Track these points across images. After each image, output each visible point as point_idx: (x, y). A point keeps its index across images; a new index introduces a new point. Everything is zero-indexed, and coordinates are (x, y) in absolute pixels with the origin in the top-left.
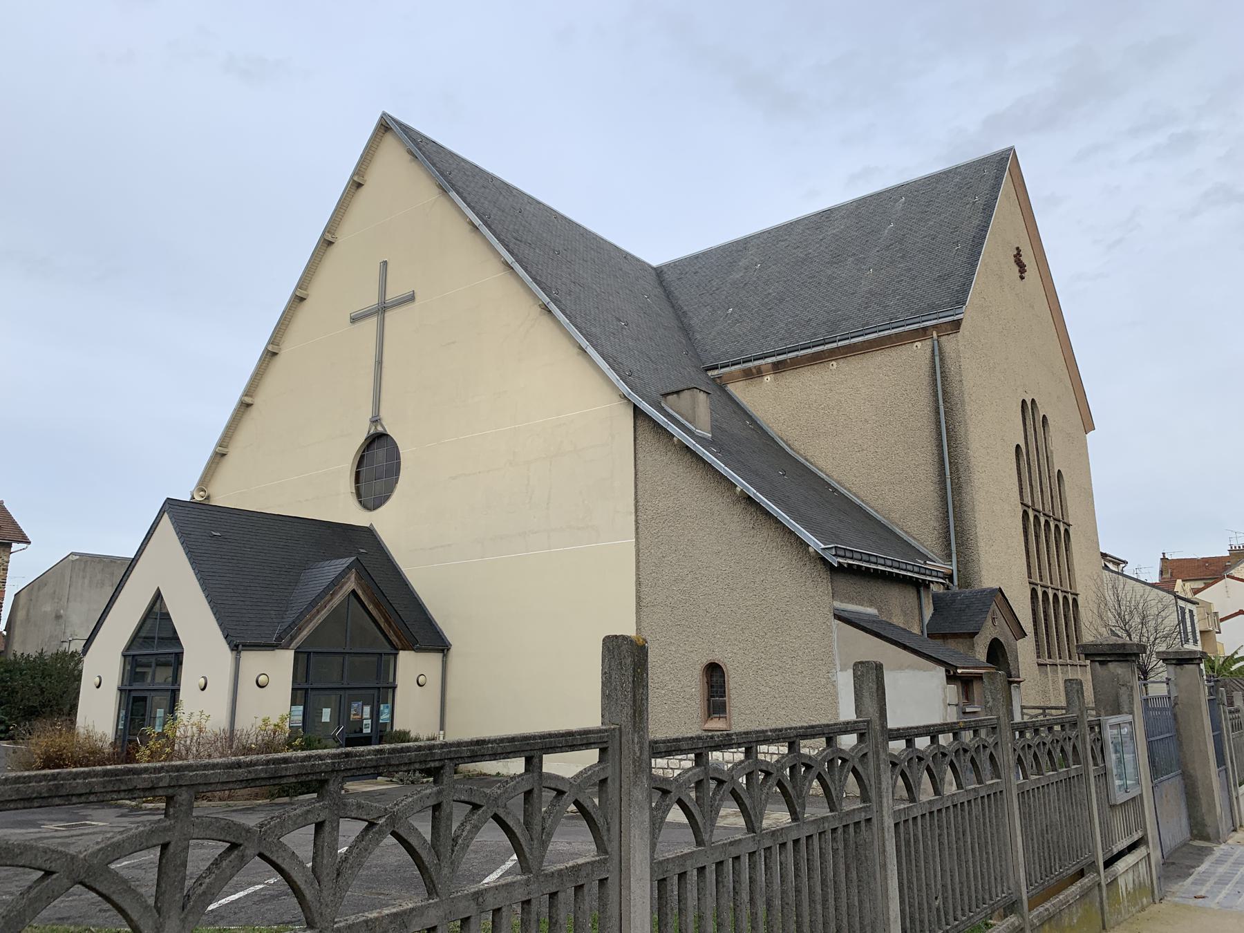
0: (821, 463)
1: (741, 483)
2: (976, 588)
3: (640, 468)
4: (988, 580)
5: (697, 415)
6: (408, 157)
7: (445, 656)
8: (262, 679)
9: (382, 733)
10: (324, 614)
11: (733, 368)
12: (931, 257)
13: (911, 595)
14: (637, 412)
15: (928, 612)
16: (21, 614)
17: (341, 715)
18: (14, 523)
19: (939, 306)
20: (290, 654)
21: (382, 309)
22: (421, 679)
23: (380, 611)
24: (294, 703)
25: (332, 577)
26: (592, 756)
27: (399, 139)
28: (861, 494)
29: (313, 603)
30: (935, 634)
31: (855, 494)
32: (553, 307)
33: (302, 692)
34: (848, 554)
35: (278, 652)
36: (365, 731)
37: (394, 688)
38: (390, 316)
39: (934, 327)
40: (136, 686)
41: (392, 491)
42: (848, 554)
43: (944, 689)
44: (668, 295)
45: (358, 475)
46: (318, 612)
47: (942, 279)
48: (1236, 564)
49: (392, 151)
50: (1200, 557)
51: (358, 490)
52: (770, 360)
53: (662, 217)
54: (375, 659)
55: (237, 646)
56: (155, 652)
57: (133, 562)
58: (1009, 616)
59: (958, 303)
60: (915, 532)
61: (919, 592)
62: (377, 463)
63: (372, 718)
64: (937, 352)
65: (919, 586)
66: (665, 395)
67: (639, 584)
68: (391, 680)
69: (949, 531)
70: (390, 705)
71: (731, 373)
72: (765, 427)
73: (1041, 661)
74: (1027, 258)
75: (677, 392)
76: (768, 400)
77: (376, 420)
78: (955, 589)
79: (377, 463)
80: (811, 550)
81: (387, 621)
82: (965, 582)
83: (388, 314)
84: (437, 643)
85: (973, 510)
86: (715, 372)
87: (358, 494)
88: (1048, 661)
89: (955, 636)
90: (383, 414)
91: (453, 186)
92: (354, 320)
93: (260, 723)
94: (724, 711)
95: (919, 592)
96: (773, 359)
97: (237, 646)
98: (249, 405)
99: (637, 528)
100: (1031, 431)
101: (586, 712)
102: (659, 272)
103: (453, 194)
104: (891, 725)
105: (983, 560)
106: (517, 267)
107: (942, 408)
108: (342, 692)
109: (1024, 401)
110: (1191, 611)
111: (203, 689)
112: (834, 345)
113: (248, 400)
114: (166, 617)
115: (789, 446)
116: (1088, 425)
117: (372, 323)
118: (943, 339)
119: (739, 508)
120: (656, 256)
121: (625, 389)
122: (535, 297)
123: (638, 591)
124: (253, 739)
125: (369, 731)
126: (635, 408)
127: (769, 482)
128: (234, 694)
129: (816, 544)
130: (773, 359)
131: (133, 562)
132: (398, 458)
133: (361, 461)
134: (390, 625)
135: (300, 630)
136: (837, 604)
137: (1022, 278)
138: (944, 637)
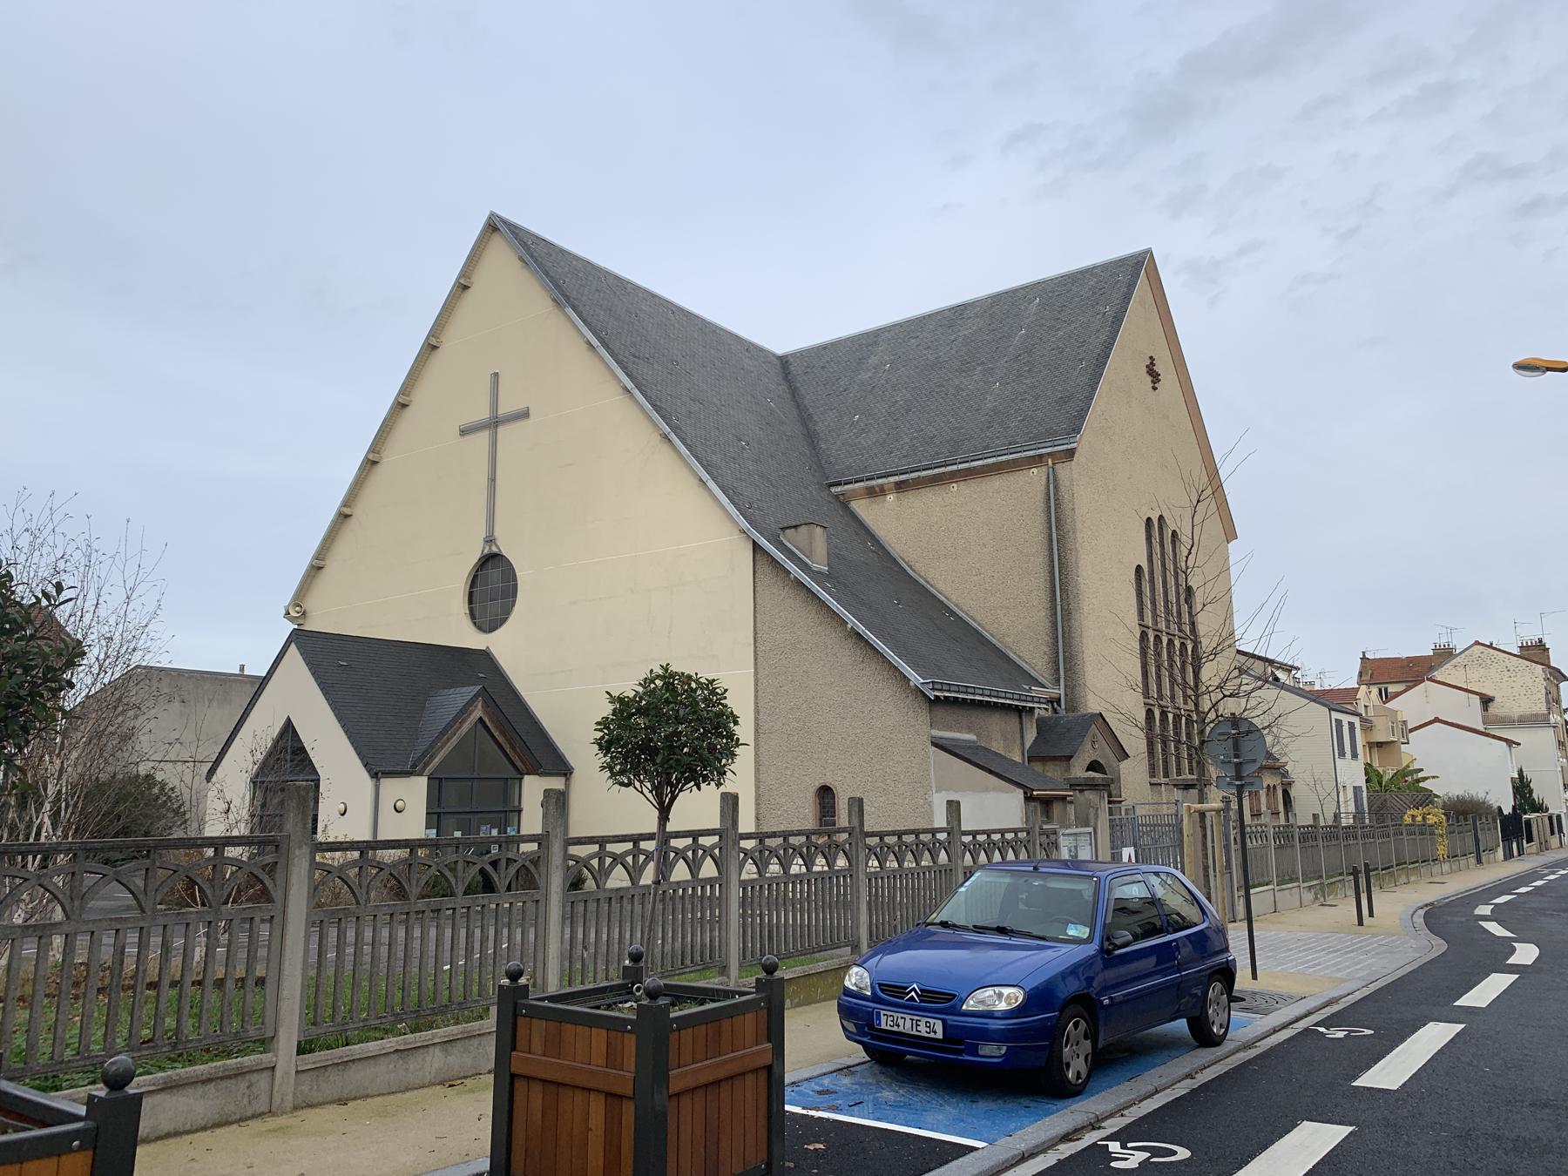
0: (941, 586)
2: (1083, 711)
4: (1093, 705)
5: (816, 546)
7: (568, 780)
13: (1013, 721)
14: (756, 547)
15: (1031, 736)
21: (494, 423)
25: (460, 704)
26: (716, 839)
28: (979, 618)
30: (1034, 757)
32: (673, 436)
33: (435, 816)
35: (414, 778)
37: (520, 811)
38: (502, 430)
39: (1049, 454)
44: (794, 391)
45: (471, 595)
47: (1063, 401)
48: (1440, 665)
49: (500, 250)
50: (1405, 655)
51: (471, 610)
52: (892, 479)
53: (790, 293)
62: (491, 586)
66: (783, 529)
73: (1154, 780)
75: (795, 527)
77: (490, 540)
78: (1062, 712)
79: (491, 586)
81: (513, 748)
82: (1072, 707)
83: (500, 429)
87: (472, 616)
88: (1163, 780)
89: (1054, 759)
92: (464, 432)
98: (347, 516)
101: (715, 822)
102: (784, 361)
103: (569, 311)
104: (867, 829)
106: (637, 393)
110: (1351, 725)
113: (347, 511)
114: (301, 750)
116: (1230, 534)
117: (483, 437)
118: (1058, 466)
119: (850, 642)
121: (745, 524)
122: (655, 424)
123: (756, 719)
129: (916, 678)
132: (515, 579)
133: (474, 581)
136: (935, 733)
137: (1155, 389)
138: (1044, 759)
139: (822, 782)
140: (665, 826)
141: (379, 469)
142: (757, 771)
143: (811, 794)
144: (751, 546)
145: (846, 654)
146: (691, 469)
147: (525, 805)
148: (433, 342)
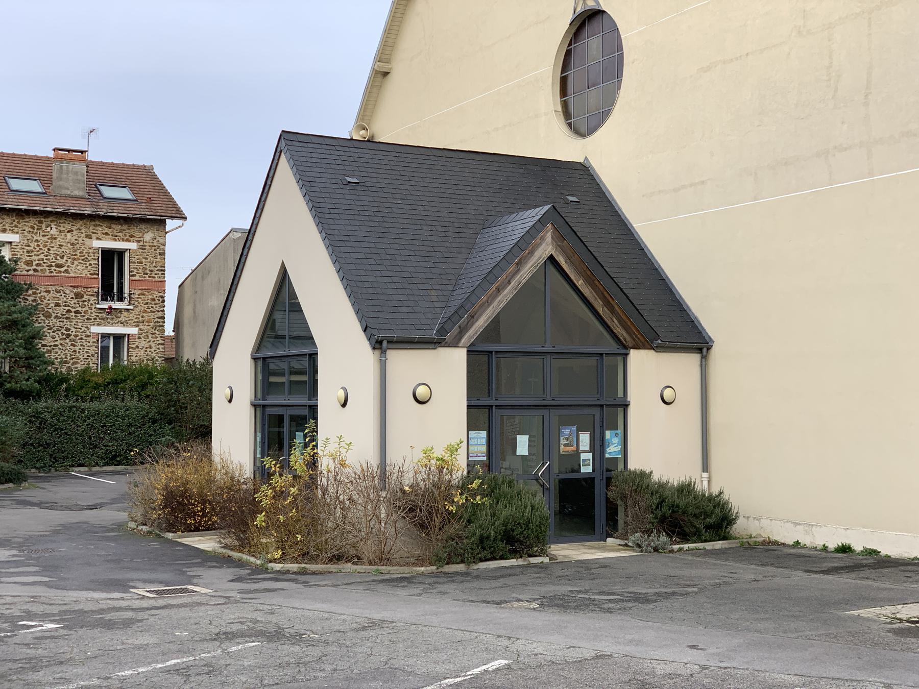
7: (704, 358)
8: (422, 391)
9: (610, 471)
10: (508, 294)
16: (188, 311)
17: (544, 445)
18: (166, 193)
20: (463, 352)
22: (668, 394)
29: (490, 277)
33: (482, 411)
36: (584, 470)
41: (613, 103)
45: (564, 82)
46: (499, 291)
51: (565, 106)
54: (592, 362)
55: (380, 342)
56: (287, 353)
57: (251, 234)
62: (588, 59)
63: (593, 449)
68: (620, 394)
70: (620, 432)
79: (588, 59)
81: (607, 304)
84: (692, 339)
87: (567, 113)
93: (418, 455)
97: (380, 342)
108: (544, 412)
111: (344, 405)
114: (296, 308)
124: (408, 480)
125: (589, 469)
128: (399, 415)
131: (251, 234)
132: (620, 47)
133: (567, 60)
134: (613, 311)
135: (473, 318)
140: (603, 452)
147: (633, 396)
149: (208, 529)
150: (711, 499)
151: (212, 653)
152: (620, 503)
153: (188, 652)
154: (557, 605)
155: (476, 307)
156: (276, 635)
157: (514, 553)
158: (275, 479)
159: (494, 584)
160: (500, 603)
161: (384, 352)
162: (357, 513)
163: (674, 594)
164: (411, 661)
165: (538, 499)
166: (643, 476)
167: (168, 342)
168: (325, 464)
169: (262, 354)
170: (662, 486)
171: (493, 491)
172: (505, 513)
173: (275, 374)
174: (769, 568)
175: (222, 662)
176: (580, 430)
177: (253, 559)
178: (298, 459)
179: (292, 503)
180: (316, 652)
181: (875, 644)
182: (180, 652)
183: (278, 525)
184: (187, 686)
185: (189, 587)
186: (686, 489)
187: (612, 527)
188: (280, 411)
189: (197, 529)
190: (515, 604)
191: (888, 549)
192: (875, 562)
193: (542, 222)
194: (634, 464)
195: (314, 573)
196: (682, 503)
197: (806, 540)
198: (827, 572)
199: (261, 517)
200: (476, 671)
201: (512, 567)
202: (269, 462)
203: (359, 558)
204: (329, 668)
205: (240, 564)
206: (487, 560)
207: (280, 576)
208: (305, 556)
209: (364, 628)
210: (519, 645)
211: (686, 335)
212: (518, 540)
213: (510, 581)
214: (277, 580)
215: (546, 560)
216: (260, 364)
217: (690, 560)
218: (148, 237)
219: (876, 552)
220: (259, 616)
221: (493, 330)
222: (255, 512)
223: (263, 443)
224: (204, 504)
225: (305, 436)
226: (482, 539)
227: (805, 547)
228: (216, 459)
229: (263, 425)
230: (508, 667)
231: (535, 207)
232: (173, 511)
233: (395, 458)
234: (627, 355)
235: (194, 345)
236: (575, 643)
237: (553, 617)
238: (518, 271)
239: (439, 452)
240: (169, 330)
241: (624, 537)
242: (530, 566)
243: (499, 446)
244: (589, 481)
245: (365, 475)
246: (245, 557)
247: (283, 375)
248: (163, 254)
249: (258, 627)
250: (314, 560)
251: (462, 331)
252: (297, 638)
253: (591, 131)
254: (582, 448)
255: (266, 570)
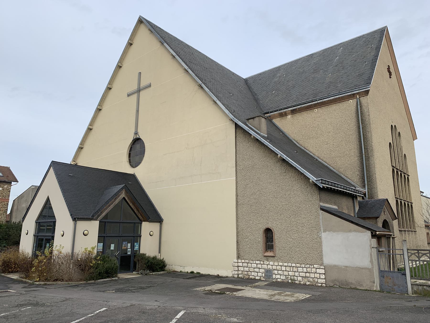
0: (311, 149)
1: (280, 154)
2: (376, 199)
3: (238, 149)
6: (149, 32)
7: (161, 224)
8: (86, 232)
9: (135, 253)
10: (112, 206)
11: (275, 113)
12: (356, 68)
14: (237, 126)
15: (357, 208)
16: (15, 208)
17: (118, 247)
19: (360, 85)
22: (151, 233)
23: (135, 206)
24: (99, 242)
25: (116, 191)
27: (146, 25)
28: (327, 161)
29: (107, 202)
31: (325, 162)
32: (203, 85)
33: (102, 238)
34: (327, 183)
35: (93, 222)
37: (140, 236)
38: (142, 93)
39: (357, 93)
40: (40, 234)
42: (327, 183)
43: (370, 240)
44: (249, 88)
46: (109, 206)
49: (143, 30)
51: (130, 160)
52: (290, 109)
53: (245, 64)
54: (132, 225)
55: (75, 219)
57: (39, 187)
58: (390, 211)
59: (367, 84)
60: (349, 176)
61: (353, 200)
62: (136, 150)
63: (131, 248)
64: (359, 104)
65: (353, 197)
67: (237, 196)
68: (139, 233)
69: (364, 176)
70: (138, 243)
71: (275, 114)
72: (288, 135)
73: (400, 229)
74: (392, 70)
75: (253, 118)
76: (290, 125)
77: (136, 133)
78: (367, 199)
79: (136, 150)
80: (311, 181)
82: (371, 196)
84: (158, 219)
85: (374, 167)
86: (268, 115)
88: (403, 229)
89: (369, 218)
90: (139, 131)
91: (166, 42)
92: (129, 95)
94: (273, 248)
95: (353, 200)
96: (292, 109)
97: (75, 219)
98: (91, 129)
99: (236, 173)
100: (394, 138)
102: (246, 81)
103: (165, 44)
105: (378, 187)
107: (361, 126)
108: (119, 238)
109: (392, 126)
111: (62, 236)
112: (316, 102)
113: (91, 127)
114: (51, 208)
115: (298, 143)
116: (415, 137)
117: (135, 96)
118: (361, 98)
119: (279, 165)
120: (245, 74)
121: (231, 116)
123: (237, 199)
124: (79, 257)
126: (236, 125)
127: (291, 157)
128: (77, 238)
129: (313, 178)
130: (292, 109)
131: (39, 187)
132: (144, 147)
135: (102, 213)
136: (322, 204)
137: (390, 77)
138: (364, 218)
139: (267, 226)
140: (134, 248)
141: (102, 112)
142: (237, 221)
143: (261, 232)
144: (234, 126)
145: (277, 169)
146: (210, 97)
148: (120, 65)
149: (16, 272)
150: (161, 260)
151: (16, 311)
152: (137, 262)
153: (8, 311)
154: (120, 291)
155: (103, 210)
156: (37, 304)
157: (108, 277)
158: (39, 257)
159: (103, 286)
160: (104, 291)
161: (76, 221)
162: (63, 267)
163: (151, 286)
164: (78, 310)
165: (116, 261)
166: (144, 255)
167: (8, 217)
168: (55, 252)
169: (38, 221)
170: (149, 257)
171: (103, 259)
172: (106, 265)
173: (42, 226)
174: (175, 278)
175: (19, 314)
176: (128, 243)
177: (30, 281)
178: (47, 251)
179: (44, 264)
180: (49, 309)
181: (200, 297)
182: (5, 311)
183: (39, 271)
184: (8, 322)
185: (9, 290)
186: (154, 258)
187: (135, 269)
188: (42, 237)
189: (12, 272)
190: (108, 291)
191: (203, 272)
192: (199, 276)
193: (122, 188)
194: (142, 252)
195: (48, 285)
196: (153, 262)
197: (183, 270)
198: (188, 279)
199: (34, 269)
200: (97, 312)
201: (107, 281)
202: (38, 252)
203: (63, 280)
204: (53, 314)
205: (25, 283)
206: (100, 279)
207: (38, 286)
208: (46, 280)
209: (64, 301)
210: (110, 303)
211: (156, 218)
212: (110, 273)
213: (107, 285)
214: (37, 287)
215: (117, 278)
216: (38, 224)
217: (155, 277)
218: (5, 186)
219: (200, 273)
220: (31, 299)
221: (106, 217)
222: (31, 267)
223: (36, 246)
224: (15, 264)
225: (50, 245)
226: (100, 273)
227: (183, 272)
228: (20, 251)
229: (37, 241)
230: (106, 310)
231: (120, 185)
232: (5, 267)
233: (76, 251)
234: (141, 223)
235: (16, 217)
236: (125, 302)
237: (119, 295)
238: (114, 201)
239: (89, 249)
240: (9, 212)
241: (138, 271)
242: (112, 280)
243: (106, 247)
244: (130, 256)
245: (66, 256)
246: (27, 280)
247: (45, 226)
248: (10, 191)
249: (31, 302)
250: (49, 281)
251: (99, 216)
252: (43, 305)
253: (136, 166)
254: (128, 248)
255: (34, 284)
